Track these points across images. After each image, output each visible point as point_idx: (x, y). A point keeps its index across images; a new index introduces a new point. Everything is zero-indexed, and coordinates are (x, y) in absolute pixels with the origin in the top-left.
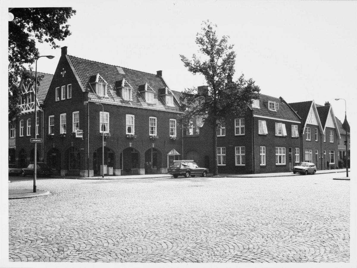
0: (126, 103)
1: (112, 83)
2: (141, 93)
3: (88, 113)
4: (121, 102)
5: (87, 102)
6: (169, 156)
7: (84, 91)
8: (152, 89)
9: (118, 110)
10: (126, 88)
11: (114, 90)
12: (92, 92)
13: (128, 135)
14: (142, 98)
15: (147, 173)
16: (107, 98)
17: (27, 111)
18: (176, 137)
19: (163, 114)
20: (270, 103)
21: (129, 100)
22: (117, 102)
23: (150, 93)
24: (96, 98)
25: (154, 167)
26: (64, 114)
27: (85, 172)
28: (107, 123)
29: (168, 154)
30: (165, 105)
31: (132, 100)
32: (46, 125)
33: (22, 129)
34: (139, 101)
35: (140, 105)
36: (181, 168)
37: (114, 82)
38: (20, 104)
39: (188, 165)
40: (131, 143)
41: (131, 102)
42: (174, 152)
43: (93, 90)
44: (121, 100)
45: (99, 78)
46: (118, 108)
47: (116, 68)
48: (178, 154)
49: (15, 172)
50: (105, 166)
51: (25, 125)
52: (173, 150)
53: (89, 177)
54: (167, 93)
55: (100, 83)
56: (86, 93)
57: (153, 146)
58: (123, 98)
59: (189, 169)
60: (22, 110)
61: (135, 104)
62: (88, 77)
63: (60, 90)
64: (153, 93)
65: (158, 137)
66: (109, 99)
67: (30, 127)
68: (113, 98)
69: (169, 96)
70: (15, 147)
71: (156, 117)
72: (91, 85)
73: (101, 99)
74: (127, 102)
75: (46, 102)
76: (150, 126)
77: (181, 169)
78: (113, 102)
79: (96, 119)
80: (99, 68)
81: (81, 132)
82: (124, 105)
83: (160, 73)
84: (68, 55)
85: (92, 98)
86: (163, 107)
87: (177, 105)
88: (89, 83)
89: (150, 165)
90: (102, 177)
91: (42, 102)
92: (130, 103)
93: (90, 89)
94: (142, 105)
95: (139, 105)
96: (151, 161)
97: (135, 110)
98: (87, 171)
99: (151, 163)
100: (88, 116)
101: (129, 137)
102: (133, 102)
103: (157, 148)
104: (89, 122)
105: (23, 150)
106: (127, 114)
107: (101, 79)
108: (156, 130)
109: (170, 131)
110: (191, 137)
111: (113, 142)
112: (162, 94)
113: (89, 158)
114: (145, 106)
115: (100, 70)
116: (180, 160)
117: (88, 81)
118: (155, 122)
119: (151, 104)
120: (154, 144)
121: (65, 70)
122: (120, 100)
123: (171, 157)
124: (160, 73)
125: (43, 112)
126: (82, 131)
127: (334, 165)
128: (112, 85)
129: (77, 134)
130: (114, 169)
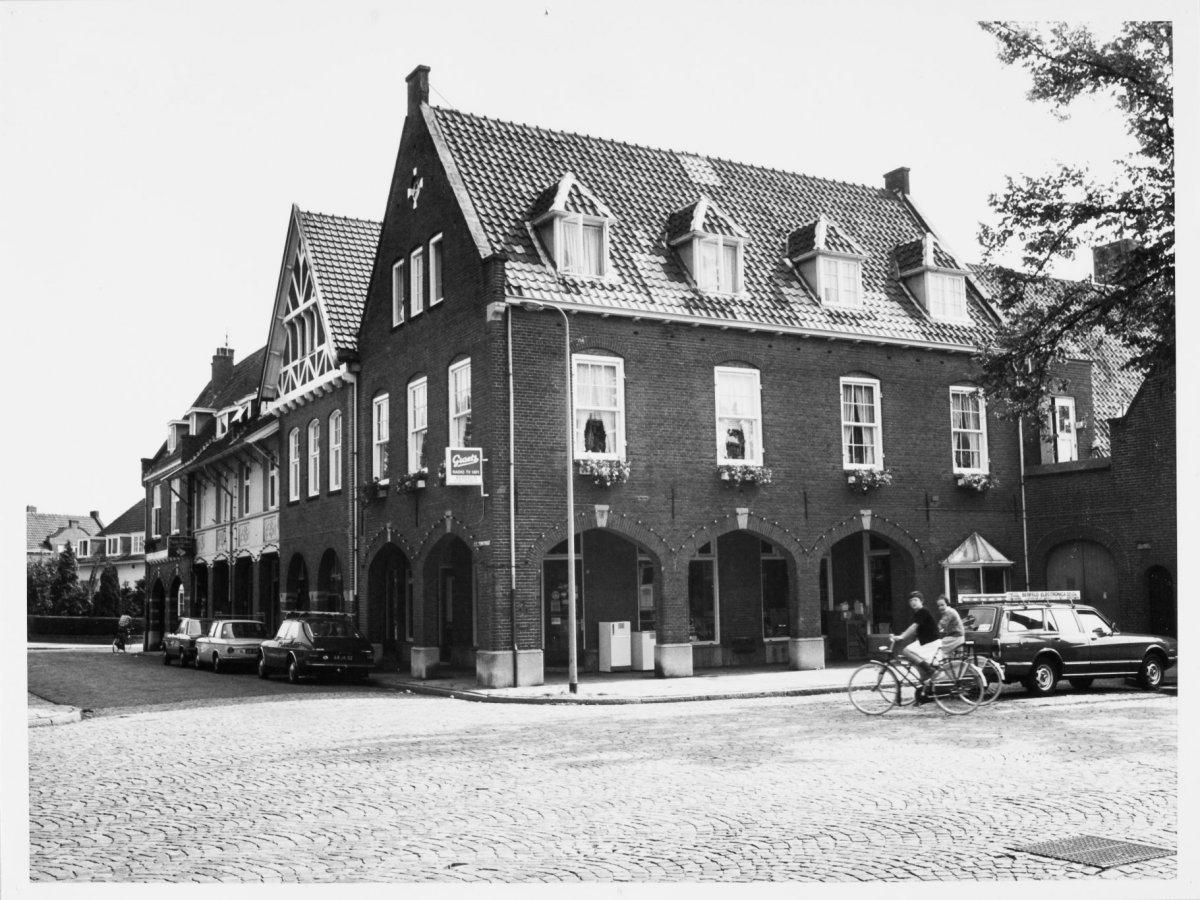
0: (714, 310)
1: (650, 224)
2: (797, 265)
4: (687, 307)
5: (500, 306)
6: (952, 572)
7: (485, 251)
8: (851, 241)
10: (711, 236)
11: (657, 250)
12: (536, 260)
13: (729, 468)
14: (805, 290)
15: (837, 656)
16: (613, 288)
17: (311, 386)
18: (988, 477)
19: (913, 360)
21: (728, 299)
22: (667, 303)
23: (840, 262)
24: (553, 287)
25: (881, 626)
27: (494, 658)
28: (613, 409)
29: (945, 562)
30: (921, 317)
31: (745, 296)
32: (364, 440)
34: (787, 302)
35: (789, 318)
36: (1000, 641)
37: (662, 219)
39: (1048, 619)
40: (746, 510)
41: (743, 305)
42: (979, 553)
43: (541, 253)
44: (689, 295)
45: (570, 194)
47: (678, 161)
48: (999, 558)
49: (248, 656)
50: (622, 626)
52: (974, 542)
53: (515, 684)
54: (929, 260)
55: (572, 215)
56: (499, 259)
57: (867, 524)
58: (700, 287)
59: (1055, 643)
61: (764, 315)
62: (523, 198)
63: (406, 272)
64: (857, 260)
65: (888, 478)
66: (622, 290)
68: (644, 285)
69: (944, 272)
71: (876, 377)
72: (535, 228)
73: (579, 293)
74: (723, 307)
75: (363, 337)
76: (844, 423)
77: (1003, 645)
78: (643, 307)
80: (591, 160)
81: (473, 459)
82: (699, 318)
83: (898, 181)
85: (529, 289)
86: (914, 328)
87: (986, 318)
88: (527, 224)
89: (857, 617)
90: (565, 687)
91: (349, 339)
92: (734, 308)
93: (529, 246)
94: (797, 318)
95: (781, 317)
96: (862, 600)
97: (762, 343)
98: (504, 655)
99: (861, 610)
100: (508, 375)
101: (732, 481)
102: (751, 306)
103: (884, 531)
105: (298, 560)
106: (720, 364)
107: (579, 195)
108: (876, 444)
109: (954, 448)
110: (1067, 472)
111: (649, 502)
112: (910, 266)
113: (514, 587)
114: (813, 323)
115: (595, 167)
116: (988, 590)
117: (521, 213)
118: (871, 400)
119: (846, 317)
120: (869, 512)
122: (684, 298)
123: (965, 578)
124: (898, 181)
125: (352, 384)
126: (477, 453)
128: (646, 231)
129: (453, 468)
130: (661, 640)
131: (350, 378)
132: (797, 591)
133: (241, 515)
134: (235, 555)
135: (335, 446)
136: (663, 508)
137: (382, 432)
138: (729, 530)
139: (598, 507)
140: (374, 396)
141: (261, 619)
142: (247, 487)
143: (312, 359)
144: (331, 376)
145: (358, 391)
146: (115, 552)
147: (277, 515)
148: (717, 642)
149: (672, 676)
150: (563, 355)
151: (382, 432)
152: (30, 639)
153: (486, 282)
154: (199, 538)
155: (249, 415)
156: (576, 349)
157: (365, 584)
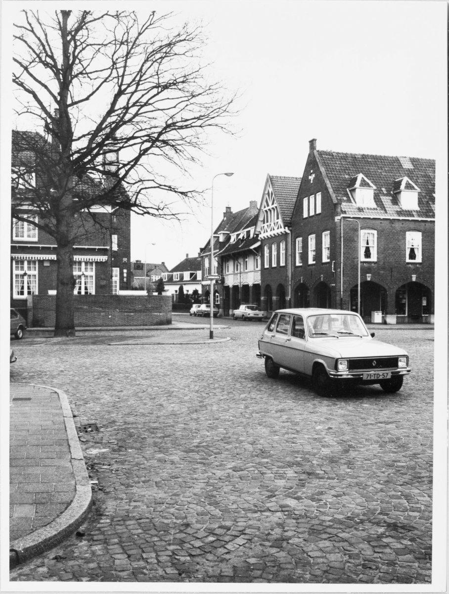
3: (341, 234)
5: (339, 218)
7: (335, 201)
9: (391, 226)
20: (16, 275)
22: (391, 213)
26: (313, 236)
46: (393, 223)
70: (260, 282)
72: (350, 191)
74: (409, 213)
79: (351, 240)
84: (318, 151)
103: (422, 281)
104: (342, 246)
105: (268, 287)
131: (288, 232)
132: (243, 325)
133: (244, 270)
134: (242, 284)
135: (282, 252)
136: (388, 275)
137: (298, 251)
138: (409, 281)
139: (368, 275)
140: (297, 238)
141: (257, 305)
142: (246, 261)
143: (274, 224)
144: (282, 230)
146: (177, 278)
147: (260, 272)
148: (406, 315)
149: (20, 76)
150: (358, 230)
151: (298, 251)
152: (11, 307)
153: (335, 210)
154: (226, 277)
155: (245, 237)
156: (362, 228)
157: (293, 295)
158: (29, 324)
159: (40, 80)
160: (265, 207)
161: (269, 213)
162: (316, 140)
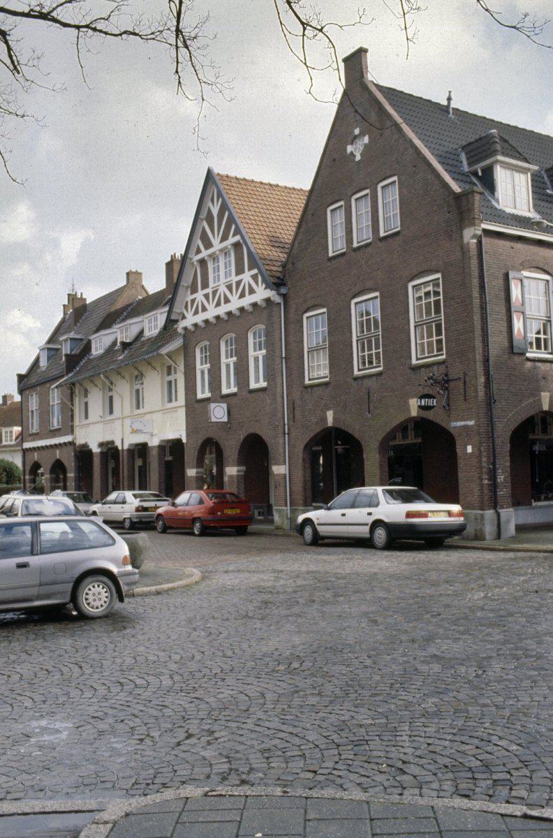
33: (228, 366)
38: (194, 290)
51: (214, 360)
60: (184, 317)
67: (209, 370)
121: (362, 134)
125: (279, 304)
127: (132, 617)
133: (132, 411)
145: (284, 308)
158: (486, 503)
159: (21, 11)
160: (199, 251)
161: (210, 266)
162: (366, 51)
